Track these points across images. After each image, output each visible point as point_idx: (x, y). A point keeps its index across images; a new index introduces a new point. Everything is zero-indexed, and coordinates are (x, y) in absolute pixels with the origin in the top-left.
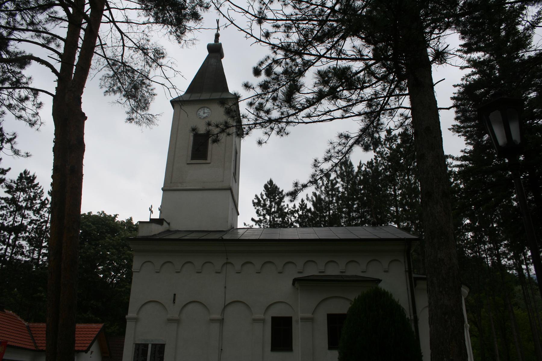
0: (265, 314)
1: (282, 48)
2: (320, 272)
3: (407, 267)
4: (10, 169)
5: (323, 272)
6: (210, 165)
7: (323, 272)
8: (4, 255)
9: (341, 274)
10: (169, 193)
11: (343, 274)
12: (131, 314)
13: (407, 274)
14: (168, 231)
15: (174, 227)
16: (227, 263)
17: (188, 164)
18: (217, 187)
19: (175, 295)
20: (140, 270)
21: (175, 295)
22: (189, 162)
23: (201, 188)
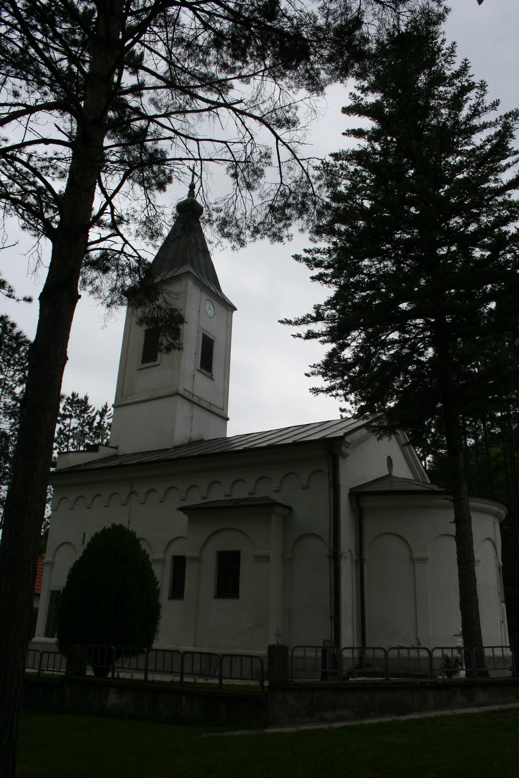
0: (165, 553)
1: (466, 100)
2: (226, 496)
3: (331, 480)
4: (292, 335)
5: (229, 496)
6: (160, 366)
7: (229, 496)
8: (515, 407)
9: (250, 496)
10: (120, 410)
11: (253, 496)
12: (48, 557)
13: (332, 489)
14: (115, 457)
15: (122, 451)
16: (131, 493)
17: (138, 370)
18: (163, 394)
19: (85, 534)
20: (57, 508)
21: (85, 534)
22: (139, 368)
23: (148, 397)
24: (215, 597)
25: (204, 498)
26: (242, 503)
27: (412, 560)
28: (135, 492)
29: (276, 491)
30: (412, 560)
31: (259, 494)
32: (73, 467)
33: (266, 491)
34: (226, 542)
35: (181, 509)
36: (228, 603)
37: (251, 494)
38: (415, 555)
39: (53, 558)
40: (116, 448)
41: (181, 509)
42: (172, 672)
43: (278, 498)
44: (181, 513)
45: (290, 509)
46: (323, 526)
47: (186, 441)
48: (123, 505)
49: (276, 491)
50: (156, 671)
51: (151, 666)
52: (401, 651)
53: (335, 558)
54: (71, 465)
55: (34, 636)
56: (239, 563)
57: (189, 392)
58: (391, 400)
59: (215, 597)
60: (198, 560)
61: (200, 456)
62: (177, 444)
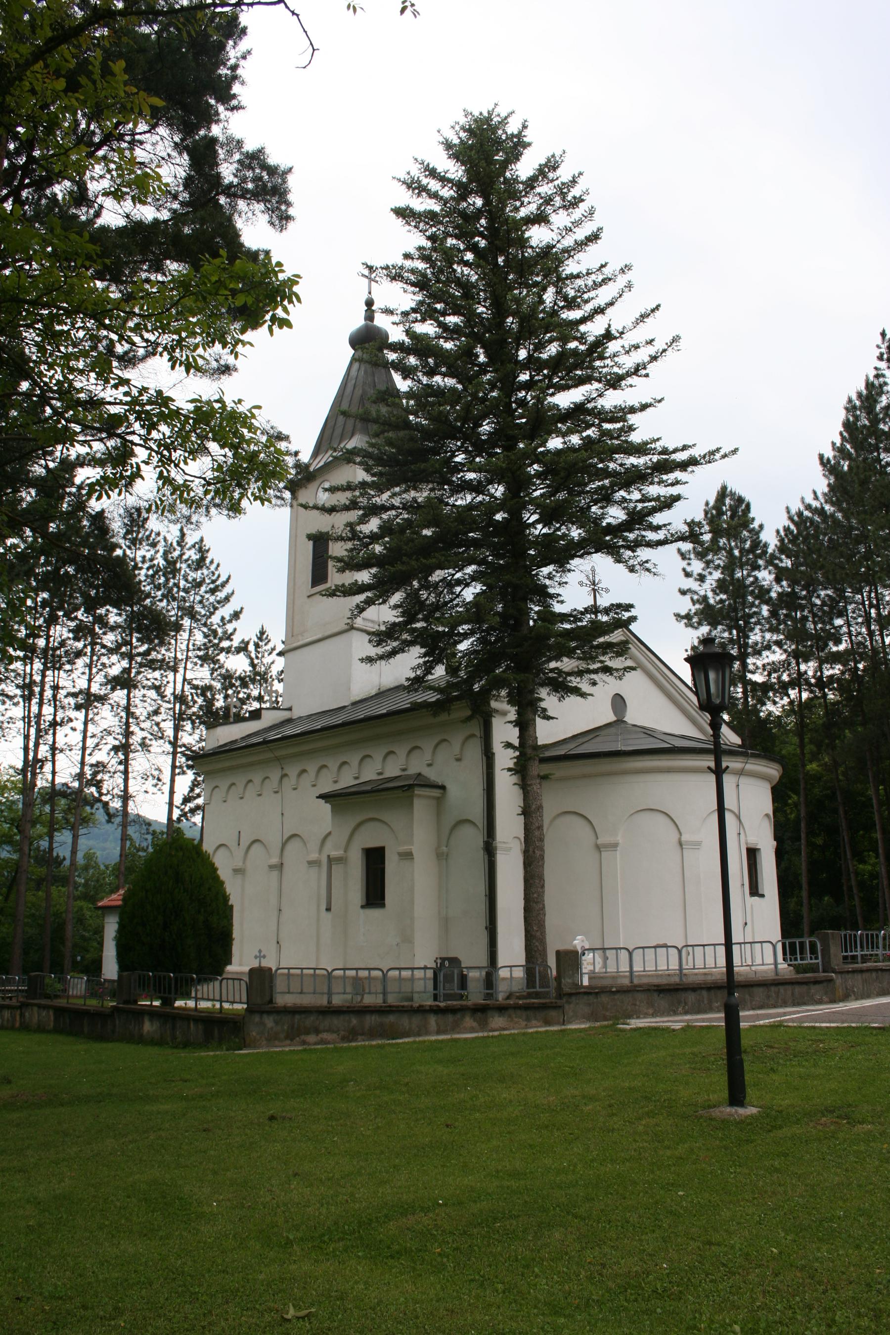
24: (362, 907)
25: (356, 778)
26: (561, 751)
27: (598, 848)
28: (286, 775)
29: (429, 765)
30: (598, 848)
31: (412, 771)
32: (225, 745)
33: (417, 766)
34: (370, 838)
35: (321, 797)
36: (374, 913)
37: (404, 770)
38: (600, 842)
39: (244, 862)
40: (290, 709)
41: (321, 797)
42: (241, 1003)
43: (432, 774)
44: (322, 801)
45: (443, 788)
46: (477, 812)
47: (373, 692)
48: (276, 792)
49: (429, 765)
50: (203, 999)
51: (199, 995)
52: (416, 972)
53: (490, 850)
54: (222, 743)
55: (229, 962)
56: (383, 862)
57: (373, 622)
58: (466, 653)
59: (362, 907)
60: (340, 860)
61: (344, 724)
62: (358, 699)
